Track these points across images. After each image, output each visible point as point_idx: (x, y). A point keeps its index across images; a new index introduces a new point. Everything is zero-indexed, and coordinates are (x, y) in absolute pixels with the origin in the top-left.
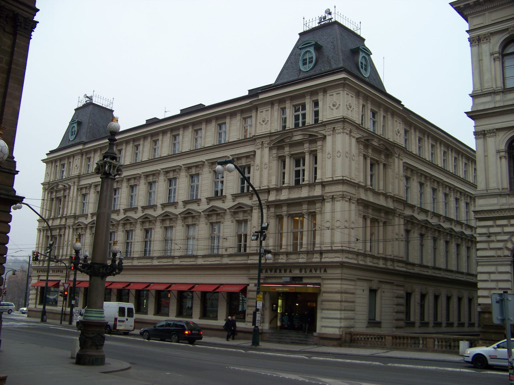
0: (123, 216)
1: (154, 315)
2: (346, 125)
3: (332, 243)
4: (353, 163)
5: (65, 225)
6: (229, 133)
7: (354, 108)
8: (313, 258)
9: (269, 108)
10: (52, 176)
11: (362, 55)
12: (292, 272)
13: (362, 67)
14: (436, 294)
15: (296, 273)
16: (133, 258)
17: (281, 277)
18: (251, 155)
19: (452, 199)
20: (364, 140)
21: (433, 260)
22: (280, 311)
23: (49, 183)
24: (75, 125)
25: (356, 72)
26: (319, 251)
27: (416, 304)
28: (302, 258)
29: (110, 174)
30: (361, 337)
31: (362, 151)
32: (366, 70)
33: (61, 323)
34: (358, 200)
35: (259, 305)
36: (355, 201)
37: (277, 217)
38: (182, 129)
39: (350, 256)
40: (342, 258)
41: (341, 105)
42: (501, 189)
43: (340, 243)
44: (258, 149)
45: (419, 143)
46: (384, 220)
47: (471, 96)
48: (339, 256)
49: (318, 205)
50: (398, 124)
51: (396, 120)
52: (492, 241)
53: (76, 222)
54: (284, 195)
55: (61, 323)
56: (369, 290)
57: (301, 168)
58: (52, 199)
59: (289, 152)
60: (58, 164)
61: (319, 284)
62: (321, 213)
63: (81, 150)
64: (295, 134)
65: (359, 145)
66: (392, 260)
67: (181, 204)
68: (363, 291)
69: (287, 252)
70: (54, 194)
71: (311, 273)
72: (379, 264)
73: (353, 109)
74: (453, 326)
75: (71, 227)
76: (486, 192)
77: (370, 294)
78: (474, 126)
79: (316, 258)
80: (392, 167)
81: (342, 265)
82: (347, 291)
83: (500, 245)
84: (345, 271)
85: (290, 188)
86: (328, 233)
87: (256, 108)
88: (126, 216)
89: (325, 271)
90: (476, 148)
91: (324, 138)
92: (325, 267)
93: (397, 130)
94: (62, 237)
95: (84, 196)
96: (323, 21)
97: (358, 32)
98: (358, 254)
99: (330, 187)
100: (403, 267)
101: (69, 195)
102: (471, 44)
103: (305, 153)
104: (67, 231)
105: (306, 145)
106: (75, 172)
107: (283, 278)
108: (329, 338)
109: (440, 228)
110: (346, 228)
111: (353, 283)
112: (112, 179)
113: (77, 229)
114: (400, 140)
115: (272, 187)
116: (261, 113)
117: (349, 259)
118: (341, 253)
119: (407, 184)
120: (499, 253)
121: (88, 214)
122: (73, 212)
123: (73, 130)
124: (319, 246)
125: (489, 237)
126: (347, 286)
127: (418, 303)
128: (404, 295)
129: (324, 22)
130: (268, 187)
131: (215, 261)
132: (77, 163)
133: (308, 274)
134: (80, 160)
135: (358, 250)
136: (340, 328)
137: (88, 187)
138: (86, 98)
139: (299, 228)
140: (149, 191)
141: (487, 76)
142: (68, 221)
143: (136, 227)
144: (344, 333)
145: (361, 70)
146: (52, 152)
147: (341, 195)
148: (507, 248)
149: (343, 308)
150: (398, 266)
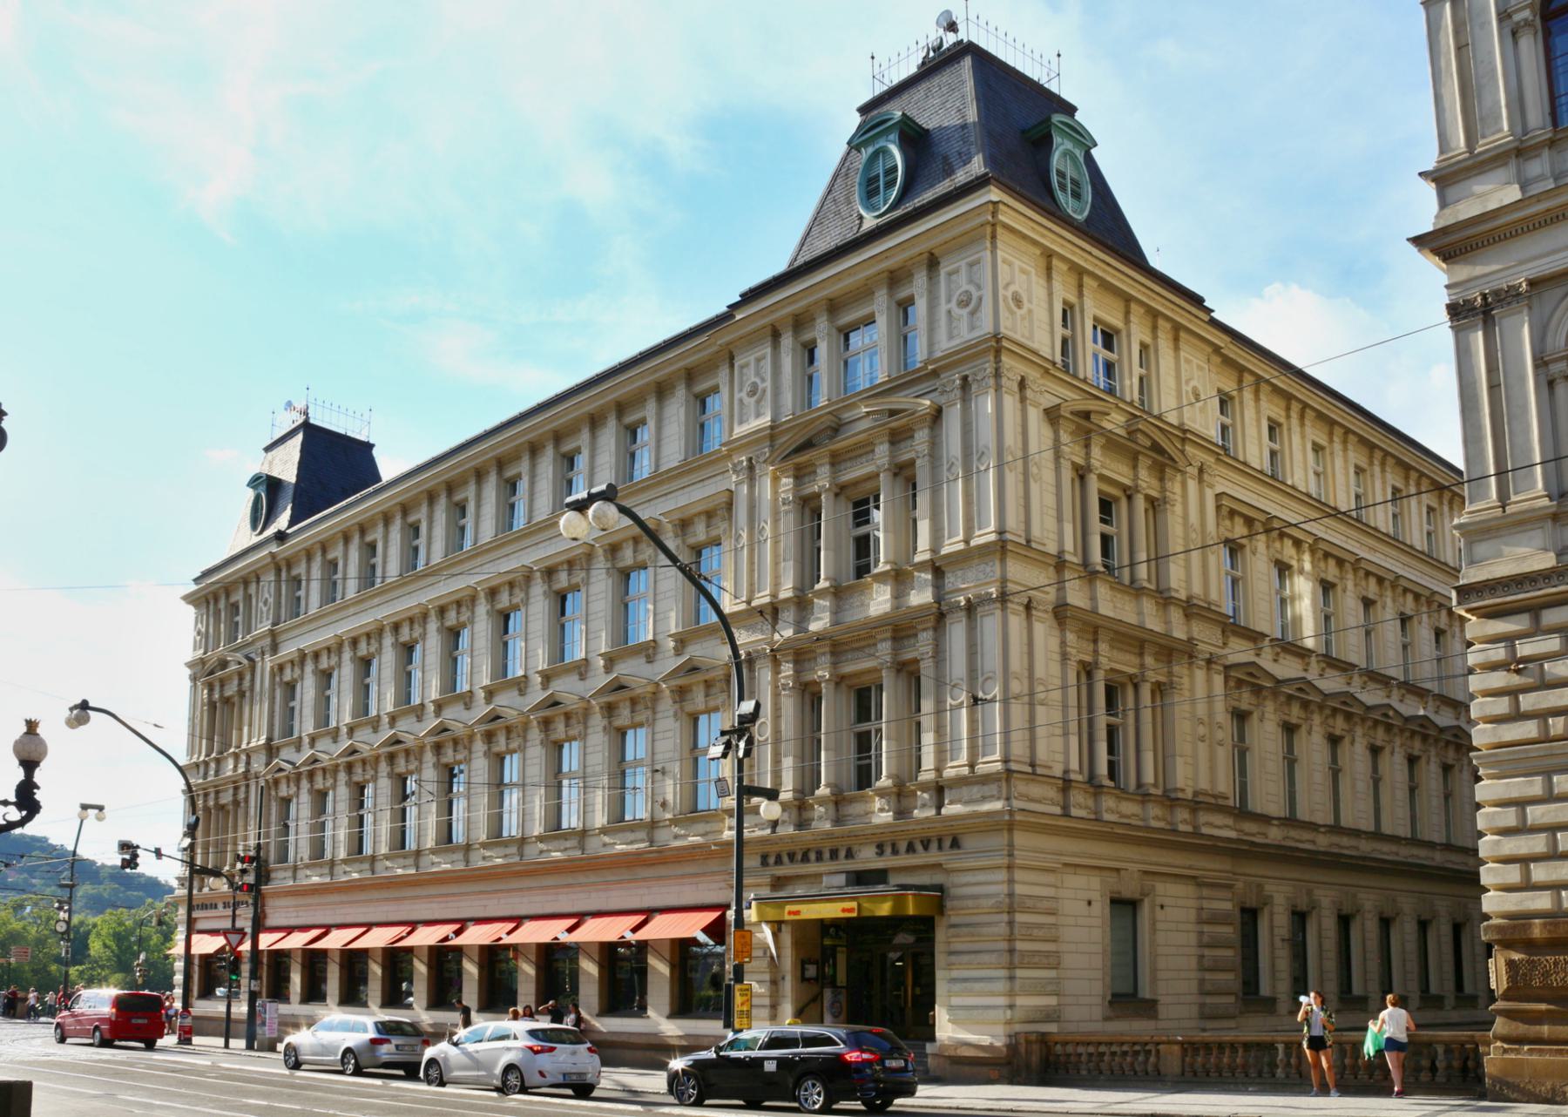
11: (1061, 148)
13: (1063, 187)
14: (1344, 912)
19: (1388, 611)
21: (1330, 806)
23: (202, 661)
27: (1278, 943)
30: (1081, 1049)
33: (227, 1046)
36: (1046, 611)
45: (1271, 439)
50: (1196, 373)
55: (227, 1046)
58: (212, 705)
68: (1089, 903)
77: (1112, 916)
78: (1447, 287)
90: (1467, 460)
93: (1190, 389)
94: (241, 812)
100: (1227, 826)
109: (1351, 706)
111: (1050, 878)
114: (1206, 422)
119: (1232, 568)
127: (1283, 940)
132: (267, 595)
133: (904, 860)
145: (1059, 194)
146: (207, 574)
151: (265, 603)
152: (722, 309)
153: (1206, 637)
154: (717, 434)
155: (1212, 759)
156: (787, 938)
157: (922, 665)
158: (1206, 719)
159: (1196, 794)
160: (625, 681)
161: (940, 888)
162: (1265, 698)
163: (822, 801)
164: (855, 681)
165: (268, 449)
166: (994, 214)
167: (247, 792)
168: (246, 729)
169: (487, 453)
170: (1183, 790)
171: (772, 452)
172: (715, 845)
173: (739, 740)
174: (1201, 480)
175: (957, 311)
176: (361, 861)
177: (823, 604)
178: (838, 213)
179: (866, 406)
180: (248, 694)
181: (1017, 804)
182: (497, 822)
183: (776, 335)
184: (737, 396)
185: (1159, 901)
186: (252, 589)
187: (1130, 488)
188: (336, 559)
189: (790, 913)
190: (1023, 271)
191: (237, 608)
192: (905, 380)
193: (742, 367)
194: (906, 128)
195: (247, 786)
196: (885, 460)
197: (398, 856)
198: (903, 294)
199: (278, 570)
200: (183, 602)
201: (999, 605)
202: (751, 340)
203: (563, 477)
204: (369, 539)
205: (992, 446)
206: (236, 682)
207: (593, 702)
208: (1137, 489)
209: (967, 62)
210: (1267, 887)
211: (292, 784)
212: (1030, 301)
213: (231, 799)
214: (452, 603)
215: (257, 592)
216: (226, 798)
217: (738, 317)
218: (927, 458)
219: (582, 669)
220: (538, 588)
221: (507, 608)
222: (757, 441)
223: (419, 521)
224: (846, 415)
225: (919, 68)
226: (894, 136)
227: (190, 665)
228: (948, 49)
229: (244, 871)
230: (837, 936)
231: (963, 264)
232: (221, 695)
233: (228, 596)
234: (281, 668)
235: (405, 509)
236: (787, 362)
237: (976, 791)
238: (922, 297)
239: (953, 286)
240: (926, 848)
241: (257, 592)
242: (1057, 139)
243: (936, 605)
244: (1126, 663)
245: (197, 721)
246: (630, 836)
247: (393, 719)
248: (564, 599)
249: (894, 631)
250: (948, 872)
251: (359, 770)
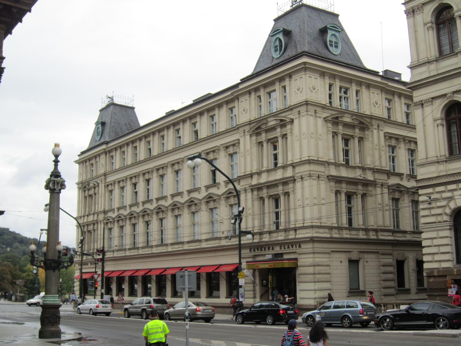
0: (187, 198)
1: (207, 298)
2: (310, 107)
3: (304, 220)
4: (320, 142)
5: (97, 220)
6: (219, 123)
7: (319, 88)
8: (263, 238)
9: (247, 97)
10: (84, 175)
11: (331, 34)
12: (274, 249)
13: (331, 45)
15: (277, 250)
16: (152, 247)
17: (265, 255)
18: (236, 144)
20: (331, 118)
22: (271, 286)
24: (100, 126)
25: (324, 52)
26: (293, 228)
28: (281, 236)
29: (55, 189)
31: (331, 129)
32: (336, 47)
34: (328, 177)
37: (260, 199)
38: (198, 117)
39: (321, 230)
40: (312, 233)
41: (304, 89)
42: (439, 157)
43: (326, 217)
44: (241, 137)
46: (361, 192)
47: (410, 68)
48: (309, 232)
49: (291, 185)
51: (373, 91)
52: (433, 208)
53: (106, 216)
54: (264, 179)
56: (348, 261)
58: (86, 197)
59: (281, 132)
60: (88, 164)
61: (296, 259)
62: (294, 191)
63: (104, 149)
64: (269, 120)
65: (327, 123)
66: (376, 231)
67: (203, 189)
68: (341, 262)
69: (269, 231)
70: (87, 192)
71: (289, 249)
72: (359, 235)
73: (318, 90)
75: (102, 222)
76: (425, 160)
79: (292, 235)
80: (370, 139)
81: (312, 240)
82: (320, 264)
83: (439, 211)
84: (316, 245)
85: (268, 171)
86: (299, 211)
87: (237, 98)
88: (189, 197)
89: (300, 246)
91: (292, 121)
92: (299, 243)
94: (96, 232)
95: (111, 191)
96: (295, 4)
98: (331, 228)
99: (299, 168)
100: (389, 236)
101: (98, 192)
102: (407, 16)
103: (278, 137)
104: (99, 225)
105: (279, 130)
106: (102, 171)
107: (266, 255)
108: (305, 309)
110: (315, 205)
112: (57, 193)
113: (107, 223)
115: (254, 171)
116: (296, 81)
117: (320, 233)
118: (311, 229)
120: (439, 219)
121: (114, 209)
122: (103, 208)
123: (99, 131)
124: (293, 223)
125: (430, 204)
126: (319, 259)
128: (395, 263)
129: (296, 5)
130: (251, 172)
131: (215, 244)
134: (104, 159)
135: (332, 224)
136: (315, 298)
137: (124, 180)
138: (108, 99)
139: (128, 277)
140: (161, 184)
141: (422, 47)
142: (100, 216)
143: (152, 218)
144: (318, 304)
145: (330, 48)
146: (83, 153)
147: (307, 174)
148: (446, 214)
149: (316, 280)
150: (382, 235)
153: (381, 178)
156: (257, 274)
158: (381, 204)
162: (404, 194)
174: (378, 129)
180: (97, 194)
184: (240, 111)
200: (74, 163)
227: (78, 184)
241: (99, 161)
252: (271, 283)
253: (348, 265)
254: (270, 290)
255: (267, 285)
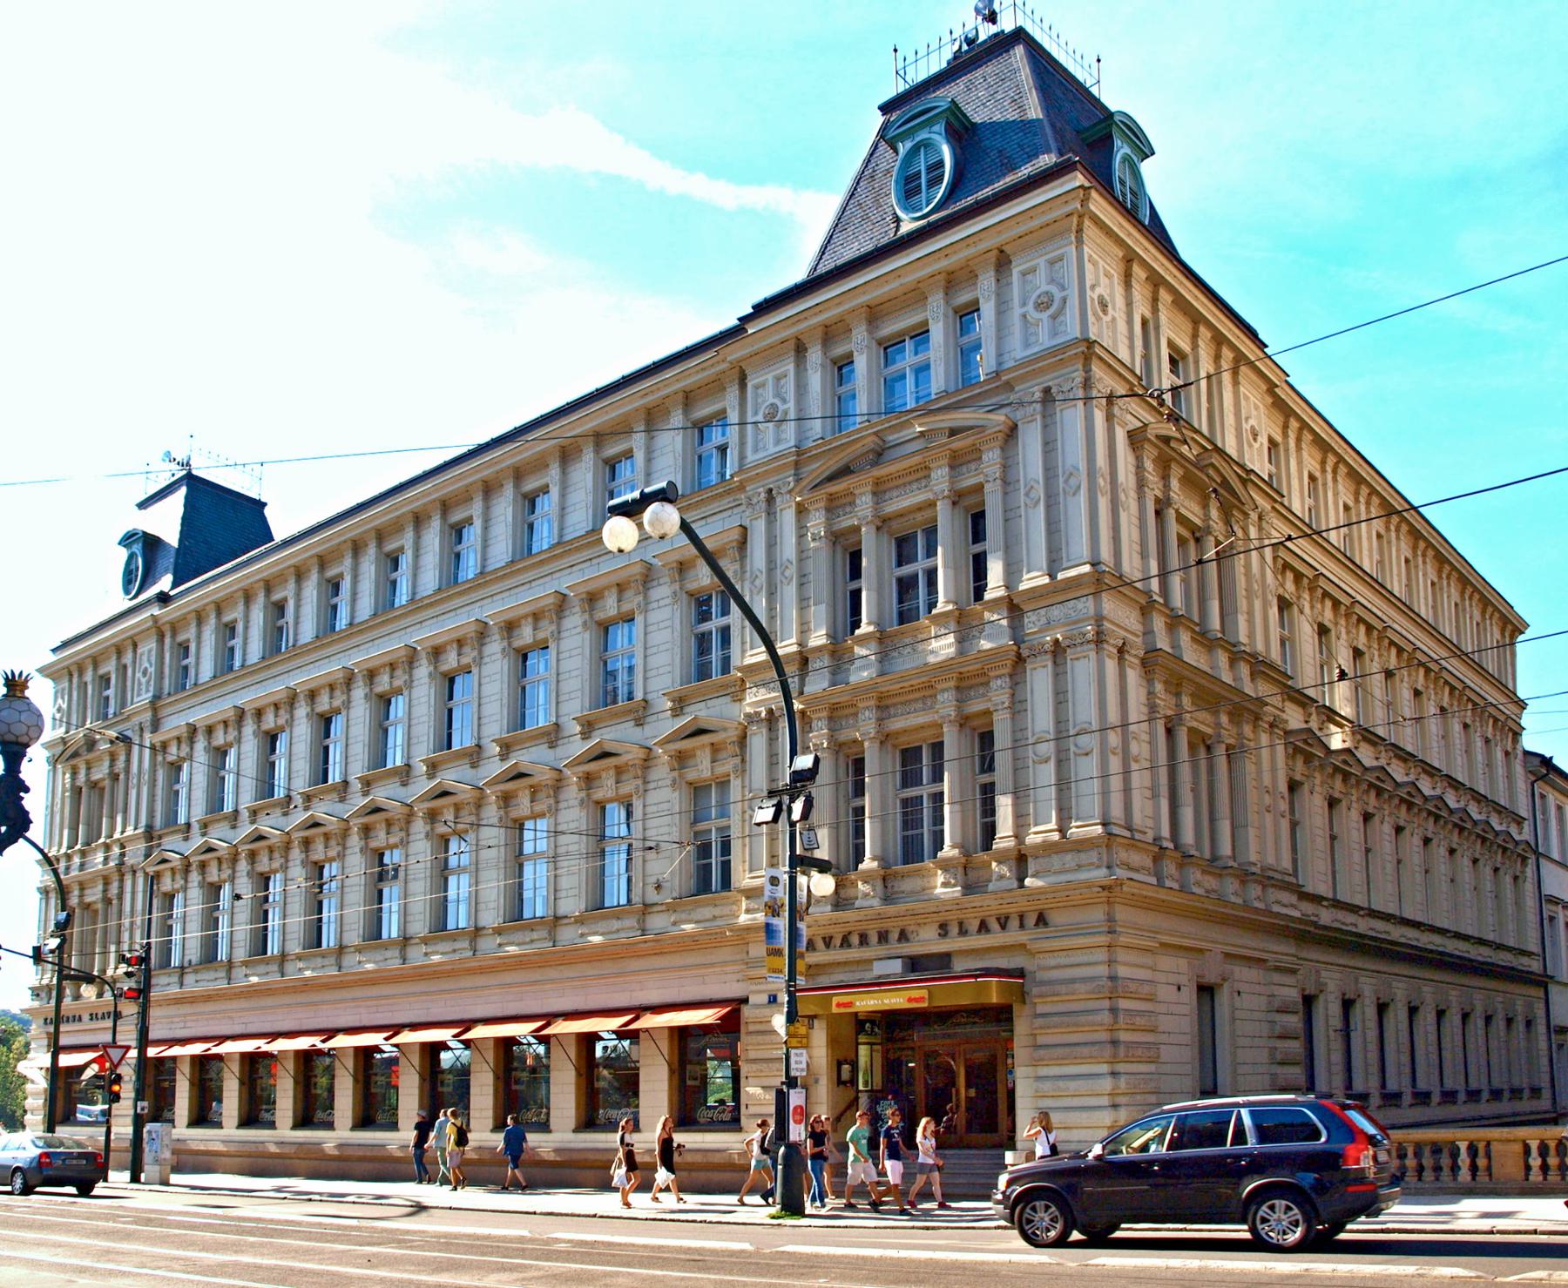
22: (866, 1084)
35: (796, 1062)
57: (919, 567)
58: (77, 792)
68: (1179, 989)
74: (1477, 1101)
97: (1094, 90)
111: (1147, 959)
132: (147, 665)
139: (925, 782)
146: (66, 644)
151: (145, 673)
152: (734, 322)
154: (545, 534)
155: (1276, 825)
157: (996, 717)
159: (1263, 869)
160: (608, 748)
161: (1020, 973)
163: (867, 878)
164: (902, 739)
165: (143, 505)
166: (1084, 202)
167: (121, 888)
168: (119, 819)
169: (430, 494)
170: (1255, 864)
171: (798, 481)
172: (731, 931)
173: (792, 800)
175: (1033, 314)
176: (268, 962)
177: (999, 619)
178: (865, 218)
179: (920, 425)
180: (122, 777)
181: (1121, 873)
182: (441, 909)
183: (800, 350)
185: (1237, 986)
186: (128, 658)
187: (1199, 528)
188: (188, 641)
189: (838, 1005)
190: (1107, 275)
191: (108, 680)
192: (966, 392)
193: (757, 387)
194: (952, 119)
195: (122, 881)
196: (869, 513)
197: (315, 956)
198: (839, 350)
199: (161, 637)
201: (1093, 646)
202: (768, 356)
203: (834, 394)
204: (227, 618)
205: (1083, 466)
206: (107, 763)
207: (567, 772)
208: (1208, 530)
209: (1019, 51)
210: (1324, 974)
211: (178, 877)
212: (1114, 309)
213: (100, 896)
214: (384, 666)
215: (134, 662)
216: (94, 895)
217: (750, 332)
218: (999, 482)
219: (405, 774)
220: (574, 620)
221: (327, 712)
222: (778, 470)
223: (285, 599)
224: (891, 438)
225: (949, 63)
226: (940, 127)
228: (985, 41)
229: (128, 974)
230: (872, 1033)
231: (1041, 262)
232: (88, 780)
233: (96, 666)
234: (165, 746)
235: (323, 562)
236: (816, 380)
237: (1069, 859)
238: (988, 299)
239: (760, 400)
240: (1003, 927)
241: (134, 662)
242: (1118, 142)
243: (1015, 648)
244: (1201, 721)
245: (58, 808)
246: (528, 936)
247: (205, 826)
248: (452, 681)
249: (880, 699)
250: (1032, 954)
251: (265, 859)
252: (865, 1072)
253: (1195, 1002)
254: (864, 1100)
255: (853, 1081)
